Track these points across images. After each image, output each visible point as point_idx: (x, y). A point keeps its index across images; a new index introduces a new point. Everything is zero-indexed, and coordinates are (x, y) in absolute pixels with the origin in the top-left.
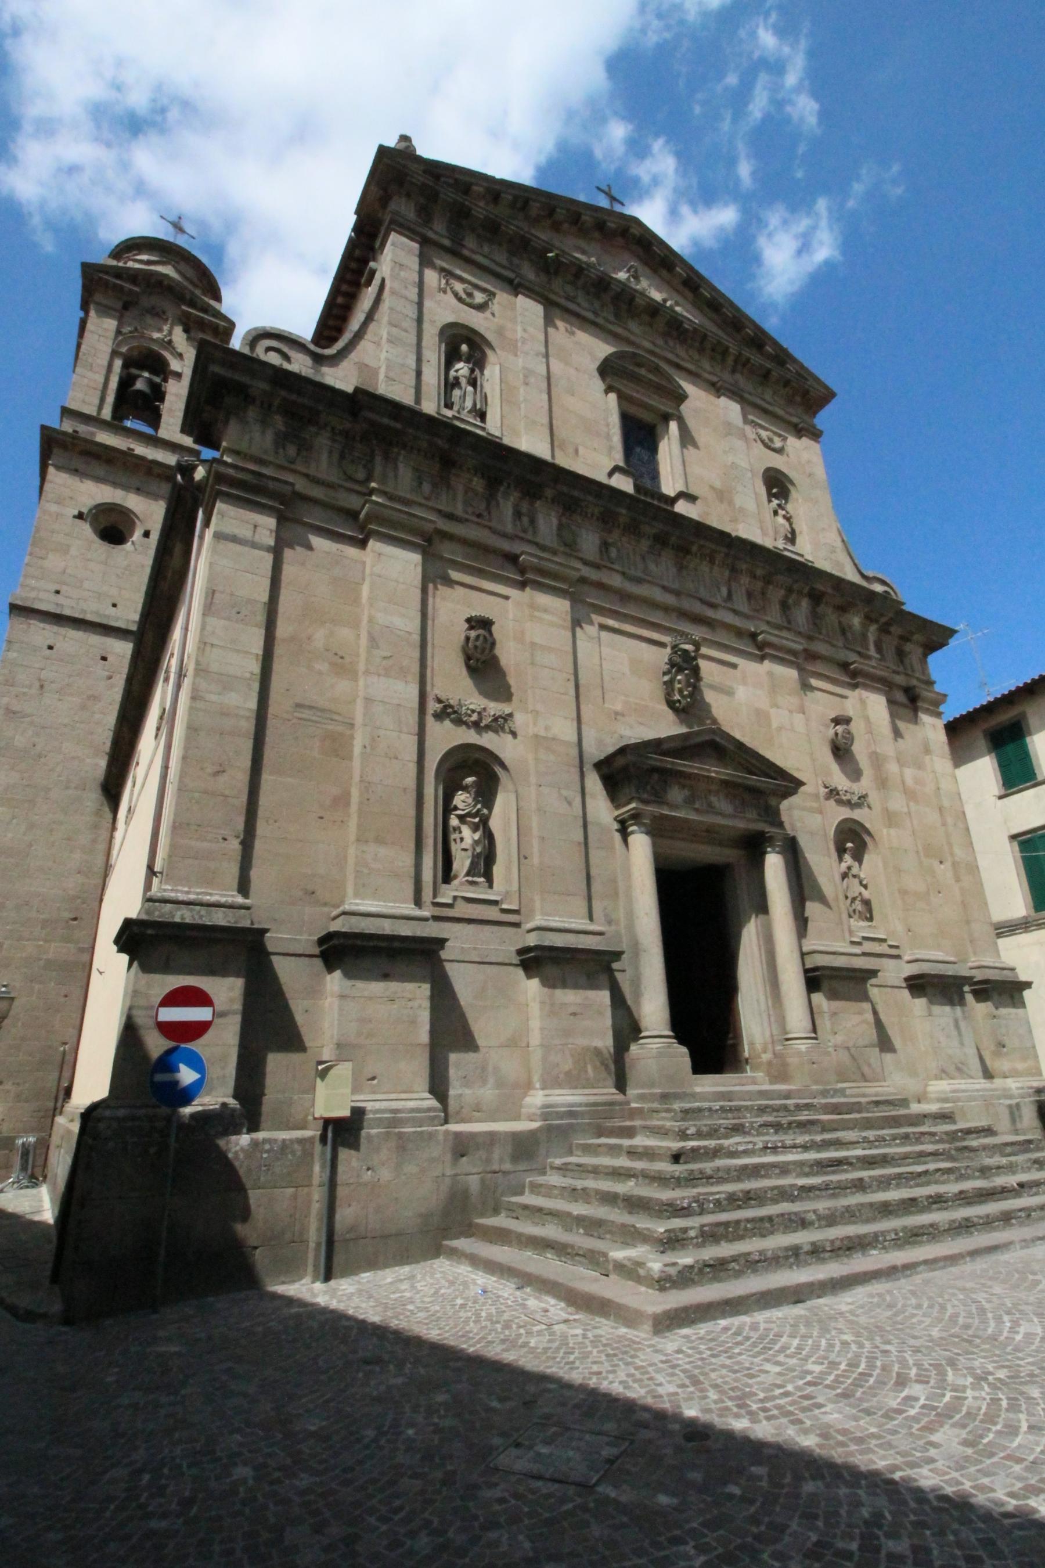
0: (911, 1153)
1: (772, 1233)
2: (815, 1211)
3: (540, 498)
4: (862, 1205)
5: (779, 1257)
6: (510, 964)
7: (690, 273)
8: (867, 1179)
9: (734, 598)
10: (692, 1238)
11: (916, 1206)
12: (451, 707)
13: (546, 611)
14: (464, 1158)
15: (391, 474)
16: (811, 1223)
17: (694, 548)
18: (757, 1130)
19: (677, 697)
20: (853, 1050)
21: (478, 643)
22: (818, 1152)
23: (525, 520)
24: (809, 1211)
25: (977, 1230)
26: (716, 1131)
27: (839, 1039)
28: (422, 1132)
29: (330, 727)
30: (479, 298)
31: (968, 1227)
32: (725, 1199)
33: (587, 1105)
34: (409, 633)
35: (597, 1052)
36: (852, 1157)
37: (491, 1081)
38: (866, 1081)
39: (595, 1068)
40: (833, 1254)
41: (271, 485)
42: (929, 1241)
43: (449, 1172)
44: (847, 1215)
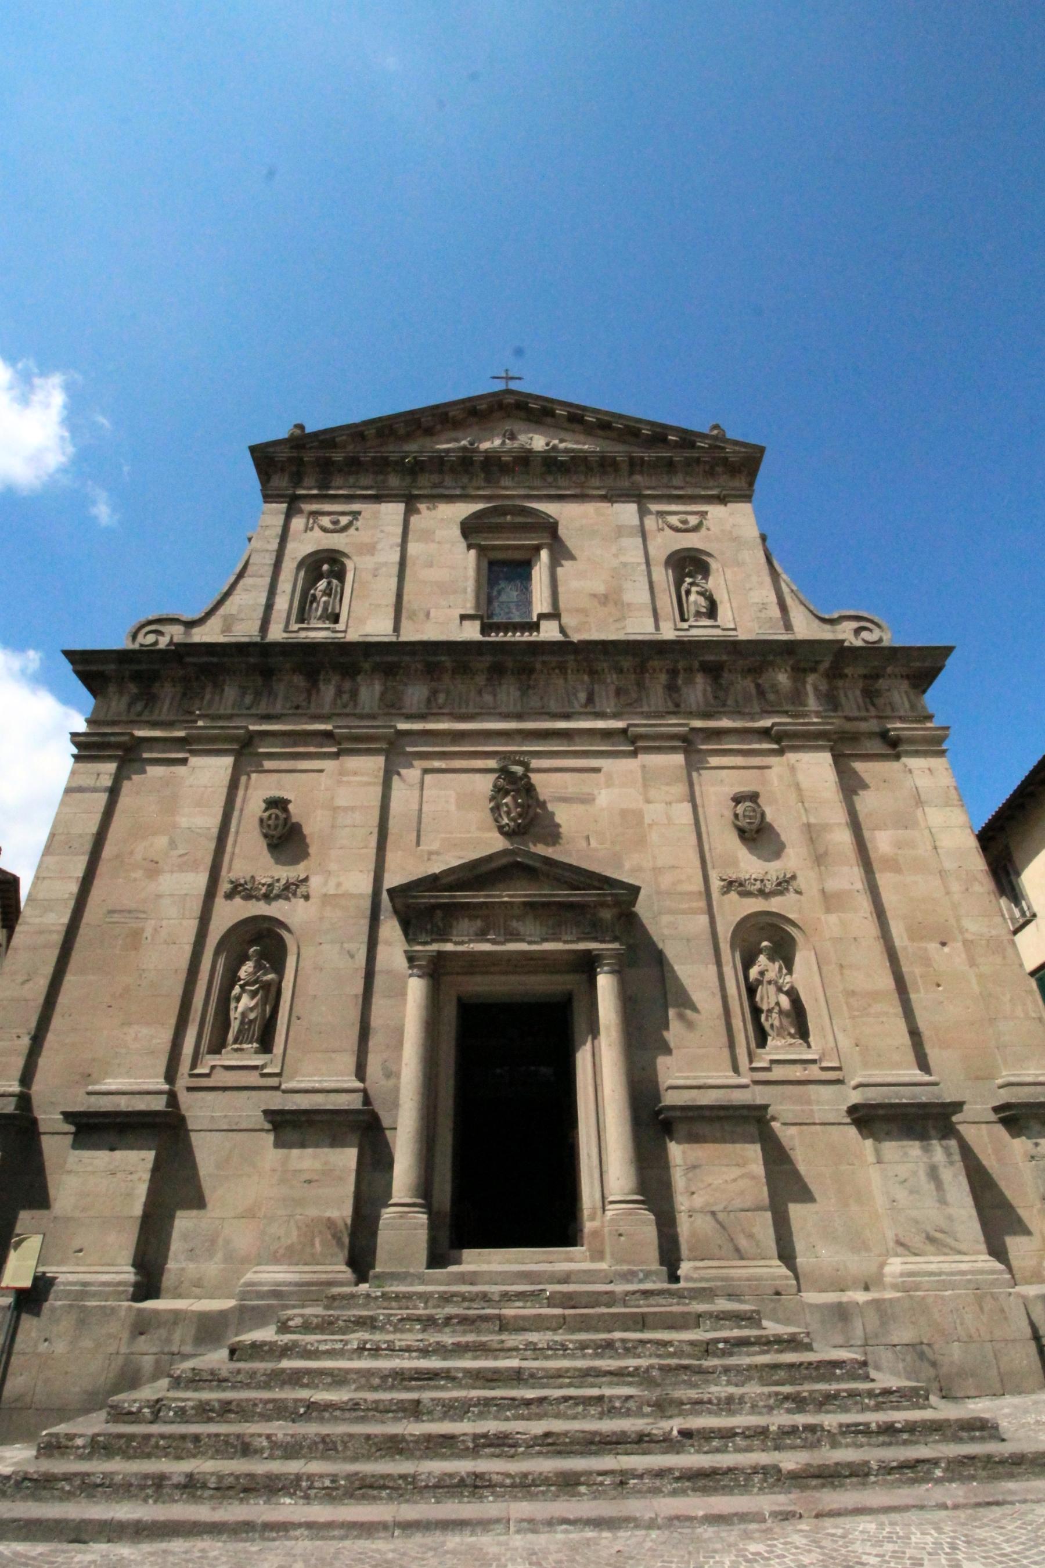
0: (568, 1370)
1: (194, 1456)
2: (268, 1437)
3: (359, 673)
4: (351, 1436)
5: (131, 1485)
6: (262, 1130)
7: (572, 410)
8: (425, 1401)
9: (597, 700)
10: (78, 1447)
11: (451, 1446)
12: (241, 885)
13: (355, 774)
14: (143, 1337)
15: (217, 698)
16: (258, 1451)
17: (538, 666)
18: (395, 1326)
19: (506, 821)
20: (721, 1216)
21: (270, 822)
22: (444, 1359)
23: (346, 697)
24: (260, 1435)
25: (493, 1494)
26: (331, 1323)
27: (698, 1201)
28: (105, 1306)
29: (134, 925)
30: (344, 520)
31: (476, 1487)
32: (193, 1408)
33: (297, 1284)
34: (209, 828)
35: (330, 1223)
36: (457, 1369)
37: (219, 1255)
38: (742, 1258)
39: (323, 1243)
40: (219, 1494)
41: (113, 739)
42: (390, 1498)
43: (123, 1350)
44: (321, 1446)
